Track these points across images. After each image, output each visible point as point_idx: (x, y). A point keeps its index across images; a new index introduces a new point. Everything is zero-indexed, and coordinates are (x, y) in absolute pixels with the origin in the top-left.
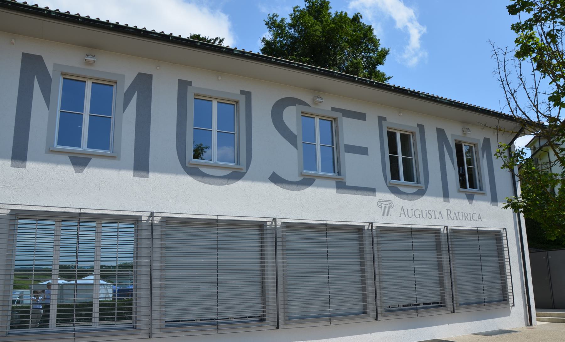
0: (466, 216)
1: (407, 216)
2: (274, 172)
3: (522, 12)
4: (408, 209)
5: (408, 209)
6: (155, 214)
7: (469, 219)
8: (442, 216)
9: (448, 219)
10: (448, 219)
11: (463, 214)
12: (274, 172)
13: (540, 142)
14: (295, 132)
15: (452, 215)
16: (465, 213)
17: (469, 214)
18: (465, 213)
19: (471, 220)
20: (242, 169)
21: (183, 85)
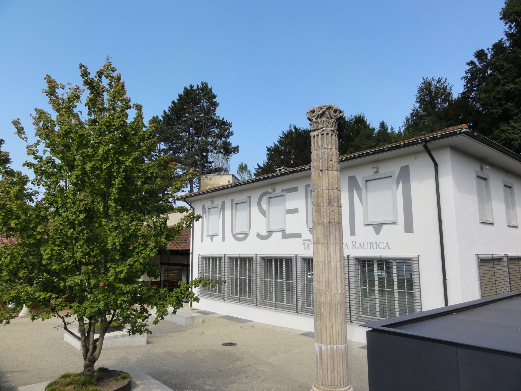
0: (354, 244)
1: (363, 248)
2: (406, 232)
3: (180, 93)
4: (364, 243)
5: (364, 243)
6: (350, 256)
7: (375, 248)
8: (388, 246)
9: (353, 249)
10: (353, 249)
11: (369, 244)
12: (406, 232)
13: (441, 180)
14: (266, 210)
15: (357, 246)
16: (370, 243)
17: (375, 244)
18: (370, 243)
19: (376, 248)
20: (353, 232)
21: (232, 200)
